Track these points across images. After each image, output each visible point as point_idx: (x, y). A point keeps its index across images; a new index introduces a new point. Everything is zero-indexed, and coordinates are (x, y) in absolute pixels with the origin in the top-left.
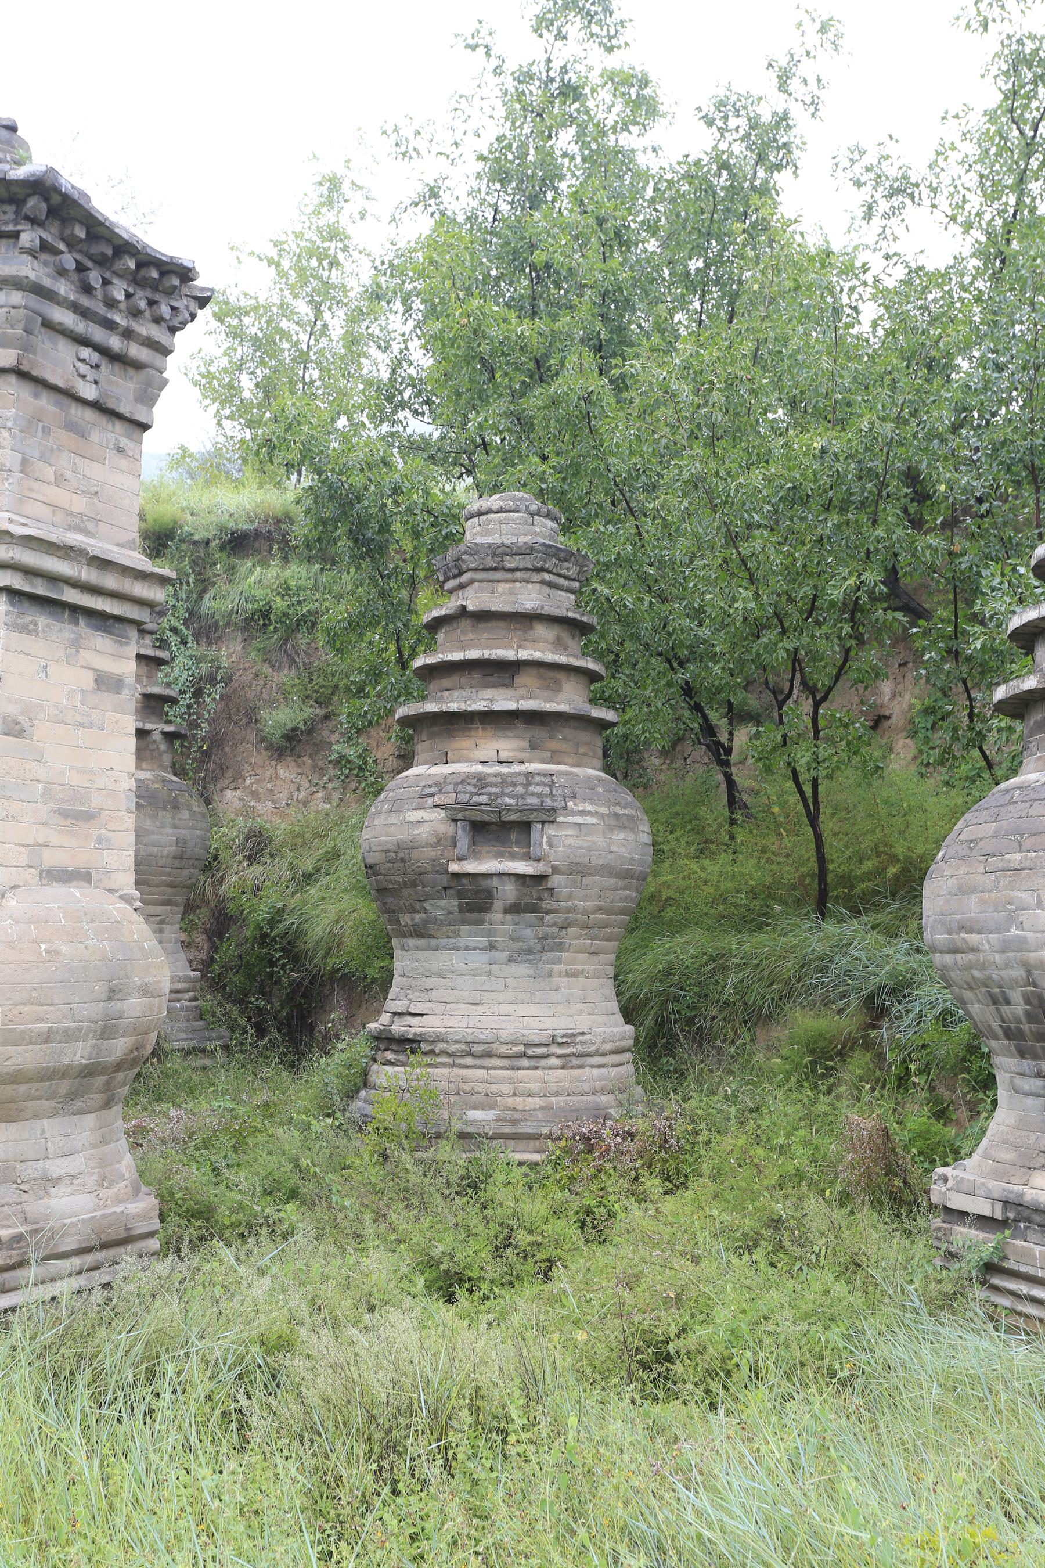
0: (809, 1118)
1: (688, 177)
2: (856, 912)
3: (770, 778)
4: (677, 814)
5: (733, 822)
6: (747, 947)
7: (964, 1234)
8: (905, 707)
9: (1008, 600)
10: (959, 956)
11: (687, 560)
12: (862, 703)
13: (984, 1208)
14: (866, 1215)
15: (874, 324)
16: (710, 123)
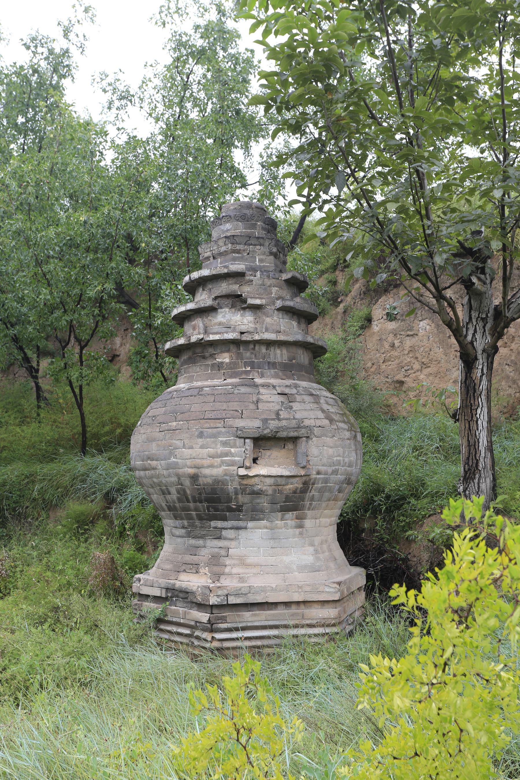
0: (75, 555)
1: (18, 74)
2: (100, 452)
3: (58, 385)
4: (10, 403)
5: (39, 407)
6: (45, 470)
7: (148, 606)
8: (127, 350)
9: (173, 301)
10: (147, 472)
11: (15, 272)
12: (105, 348)
13: (157, 592)
14: (101, 601)
15: (113, 161)
16: (28, 48)
